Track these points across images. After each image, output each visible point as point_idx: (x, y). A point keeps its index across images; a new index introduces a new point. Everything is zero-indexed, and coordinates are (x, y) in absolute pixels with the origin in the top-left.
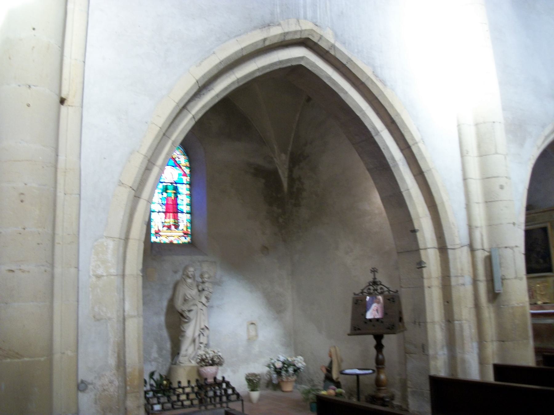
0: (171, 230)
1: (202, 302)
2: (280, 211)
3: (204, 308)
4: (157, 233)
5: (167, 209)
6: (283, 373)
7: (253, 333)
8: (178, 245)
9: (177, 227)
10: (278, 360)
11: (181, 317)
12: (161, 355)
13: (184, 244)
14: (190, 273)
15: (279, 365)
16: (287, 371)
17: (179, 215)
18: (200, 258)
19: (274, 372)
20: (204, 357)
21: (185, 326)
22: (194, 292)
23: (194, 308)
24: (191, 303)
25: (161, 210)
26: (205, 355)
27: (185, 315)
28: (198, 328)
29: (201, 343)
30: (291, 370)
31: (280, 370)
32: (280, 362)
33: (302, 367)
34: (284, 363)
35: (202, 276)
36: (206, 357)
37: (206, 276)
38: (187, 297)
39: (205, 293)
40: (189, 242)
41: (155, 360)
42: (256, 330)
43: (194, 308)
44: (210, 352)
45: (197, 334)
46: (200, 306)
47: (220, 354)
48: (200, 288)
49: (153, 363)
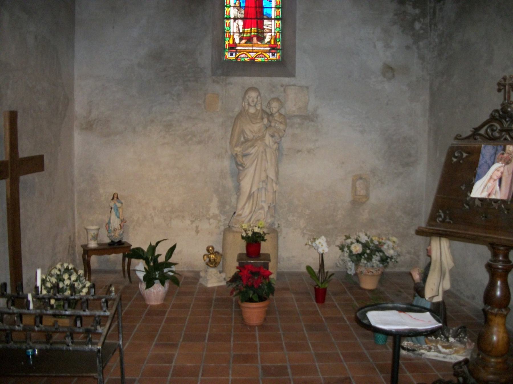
0: (252, 43)
2: (417, 11)
4: (233, 47)
5: (246, 14)
9: (261, 39)
10: (358, 241)
13: (270, 63)
17: (266, 22)
25: (238, 16)
32: (360, 245)
33: (395, 256)
34: (365, 246)
41: (215, 217)
42: (367, 189)
49: (212, 221)
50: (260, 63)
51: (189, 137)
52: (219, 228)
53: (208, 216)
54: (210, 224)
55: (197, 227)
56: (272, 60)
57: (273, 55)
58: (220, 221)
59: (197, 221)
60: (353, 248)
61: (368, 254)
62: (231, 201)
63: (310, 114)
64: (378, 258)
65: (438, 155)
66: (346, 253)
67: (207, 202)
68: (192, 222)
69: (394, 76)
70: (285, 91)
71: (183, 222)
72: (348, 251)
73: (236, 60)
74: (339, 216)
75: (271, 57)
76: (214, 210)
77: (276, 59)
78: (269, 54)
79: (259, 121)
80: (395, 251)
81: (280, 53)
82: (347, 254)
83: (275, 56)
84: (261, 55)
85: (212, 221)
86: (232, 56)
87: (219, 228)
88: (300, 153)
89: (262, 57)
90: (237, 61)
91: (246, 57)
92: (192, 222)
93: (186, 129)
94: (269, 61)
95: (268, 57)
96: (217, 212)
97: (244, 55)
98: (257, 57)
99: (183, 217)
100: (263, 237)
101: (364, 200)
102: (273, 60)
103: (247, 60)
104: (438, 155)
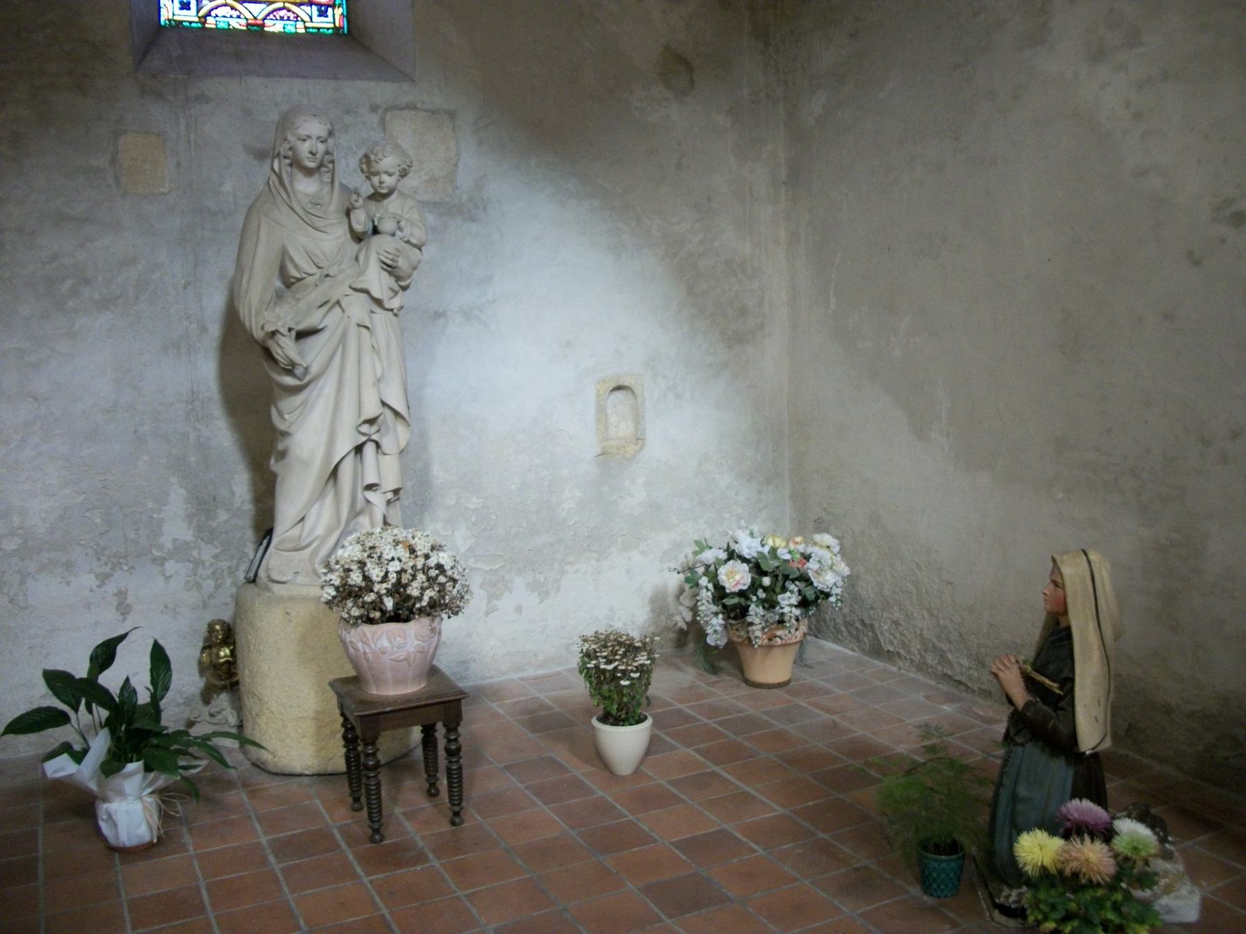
1: (366, 292)
3: (380, 315)
6: (756, 612)
7: (622, 428)
8: (284, 39)
11: (266, 365)
12: (206, 533)
13: (313, 39)
14: (304, 149)
15: (736, 577)
16: (770, 604)
18: (383, 91)
19: (714, 608)
20: (356, 578)
21: (288, 404)
22: (333, 239)
23: (332, 320)
24: (315, 296)
26: (362, 564)
27: (277, 352)
28: (348, 418)
29: (370, 487)
30: (788, 601)
31: (742, 601)
35: (368, 166)
36: (366, 578)
37: (389, 162)
38: (296, 267)
39: (381, 246)
40: (337, 30)
41: (180, 551)
42: (638, 418)
43: (332, 320)
44: (388, 552)
45: (344, 445)
46: (357, 308)
47: (444, 558)
48: (360, 221)
49: (171, 566)
50: (283, 38)
51: (68, 283)
52: (198, 586)
53: (156, 553)
54: (167, 579)
55: (122, 594)
56: (319, 29)
57: (322, 14)
58: (198, 563)
59: (118, 574)
60: (724, 575)
61: (765, 589)
62: (233, 493)
63: (465, 197)
64: (795, 599)
65: (833, 306)
66: (705, 590)
67: (150, 505)
68: (103, 579)
69: (692, 83)
70: (382, 123)
71: (68, 583)
72: (710, 586)
73: (199, 25)
74: (565, 505)
75: (315, 18)
76: (176, 529)
77: (332, 25)
78: (307, 9)
79: (334, 221)
80: (836, 573)
81: (345, 6)
82: (709, 594)
83: (327, 16)
84: (283, 13)
85: (171, 566)
86: (185, 12)
87: (198, 586)
88: (442, 320)
89: (285, 18)
90: (204, 29)
91: (235, 16)
92: (103, 579)
93: (54, 258)
94: (311, 30)
95: (307, 18)
96: (186, 534)
97: (228, 8)
98: (271, 16)
99: (69, 565)
100: (388, 592)
101: (631, 449)
102: (324, 28)
103: (237, 26)
104: (833, 306)
